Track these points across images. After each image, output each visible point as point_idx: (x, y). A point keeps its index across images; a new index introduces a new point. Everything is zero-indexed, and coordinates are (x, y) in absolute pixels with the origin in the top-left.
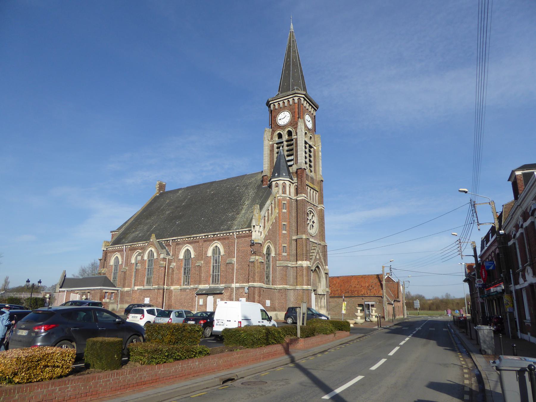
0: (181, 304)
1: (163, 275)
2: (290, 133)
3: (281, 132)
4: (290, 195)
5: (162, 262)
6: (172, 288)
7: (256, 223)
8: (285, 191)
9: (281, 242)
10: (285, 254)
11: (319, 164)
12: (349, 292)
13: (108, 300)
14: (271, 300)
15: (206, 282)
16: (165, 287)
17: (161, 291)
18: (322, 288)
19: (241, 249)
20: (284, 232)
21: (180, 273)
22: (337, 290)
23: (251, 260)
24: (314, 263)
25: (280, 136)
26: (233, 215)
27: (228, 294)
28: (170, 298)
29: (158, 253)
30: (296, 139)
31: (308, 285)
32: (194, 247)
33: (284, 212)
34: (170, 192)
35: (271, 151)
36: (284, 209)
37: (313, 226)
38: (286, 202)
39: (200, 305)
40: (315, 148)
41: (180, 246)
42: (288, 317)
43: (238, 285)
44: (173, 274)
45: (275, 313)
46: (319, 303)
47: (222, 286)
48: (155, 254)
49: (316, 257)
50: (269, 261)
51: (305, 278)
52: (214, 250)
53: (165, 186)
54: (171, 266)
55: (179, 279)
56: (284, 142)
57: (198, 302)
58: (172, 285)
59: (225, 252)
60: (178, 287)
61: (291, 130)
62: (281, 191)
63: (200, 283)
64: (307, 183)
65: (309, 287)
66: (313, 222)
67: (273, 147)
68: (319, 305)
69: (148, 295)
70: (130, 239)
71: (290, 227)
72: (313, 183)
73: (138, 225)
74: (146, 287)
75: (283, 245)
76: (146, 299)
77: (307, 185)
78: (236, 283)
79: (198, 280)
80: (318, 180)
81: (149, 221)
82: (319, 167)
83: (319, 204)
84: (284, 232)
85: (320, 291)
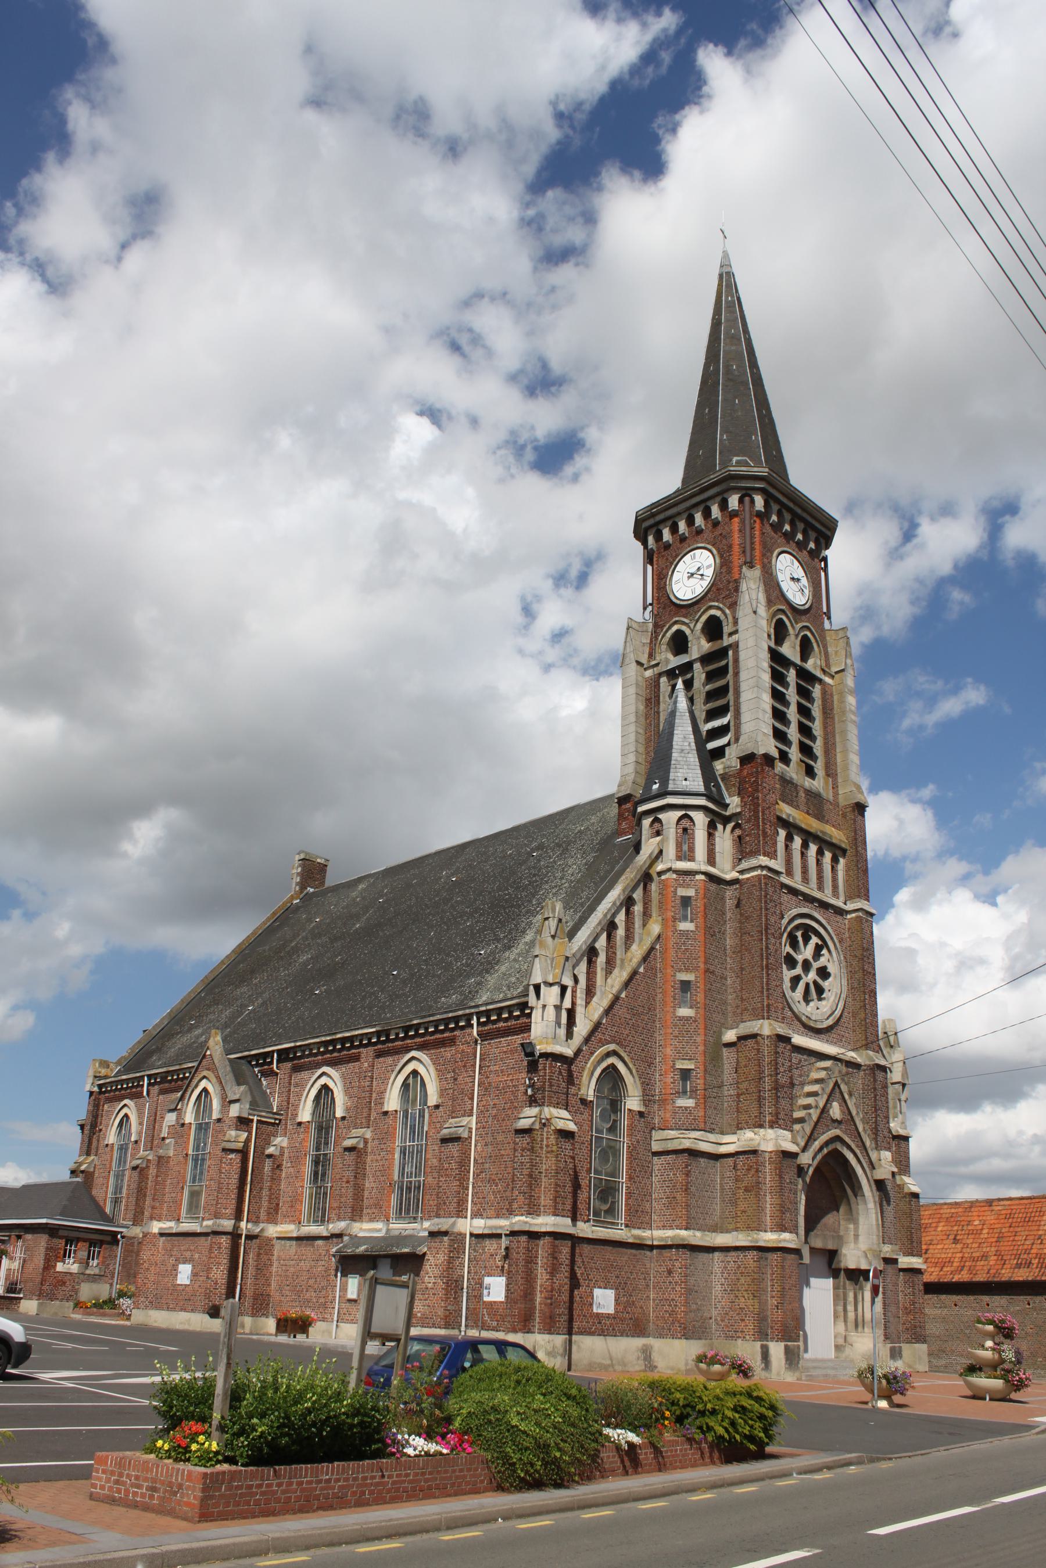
0: (298, 1293)
1: (234, 1181)
2: (713, 629)
3: (684, 628)
4: (711, 860)
5: (233, 1133)
6: (273, 1231)
7: (544, 972)
8: (692, 849)
9: (669, 1051)
10: (690, 1103)
11: (845, 740)
12: (1029, 1264)
13: (75, 1268)
14: (619, 1288)
15: (380, 1213)
16: (243, 1224)
17: (225, 1241)
18: (864, 1244)
19: (493, 1078)
20: (684, 1012)
21: (299, 1175)
22: (985, 1257)
23: (524, 1124)
24: (811, 1139)
25: (680, 644)
26: (493, 953)
27: (442, 1258)
28: (262, 1270)
29: (224, 1097)
30: (735, 646)
31: (782, 1228)
32: (343, 1077)
33: (685, 933)
34: (336, 889)
35: (648, 701)
36: (685, 918)
37: (820, 991)
38: (690, 892)
39: (350, 1301)
40: (827, 680)
41: (304, 1075)
42: (983, 1346)
43: (480, 1225)
44: (275, 1179)
45: (638, 1342)
46: (850, 1308)
47: (423, 1227)
48: (216, 1104)
49: (824, 1110)
50: (612, 1129)
51: (769, 1202)
52: (405, 1085)
53: (323, 868)
54: (271, 1150)
55: (296, 1199)
56: (697, 666)
57: (344, 1289)
58: (272, 1219)
59: (442, 1092)
60: (292, 1227)
61: (718, 613)
62: (671, 850)
63: (356, 1213)
64: (786, 810)
65: (786, 1235)
66: (823, 973)
67: (657, 685)
68: (851, 1315)
69: (188, 1254)
70: (172, 1052)
71: (708, 991)
72: (820, 817)
73: (209, 1006)
74: (186, 1226)
75: (680, 1065)
76: (181, 1267)
77: (785, 823)
78: (476, 1215)
79: (350, 1201)
80: (842, 802)
81: (245, 989)
82: (845, 751)
83: (849, 898)
84: (684, 1012)
85: (852, 1257)
